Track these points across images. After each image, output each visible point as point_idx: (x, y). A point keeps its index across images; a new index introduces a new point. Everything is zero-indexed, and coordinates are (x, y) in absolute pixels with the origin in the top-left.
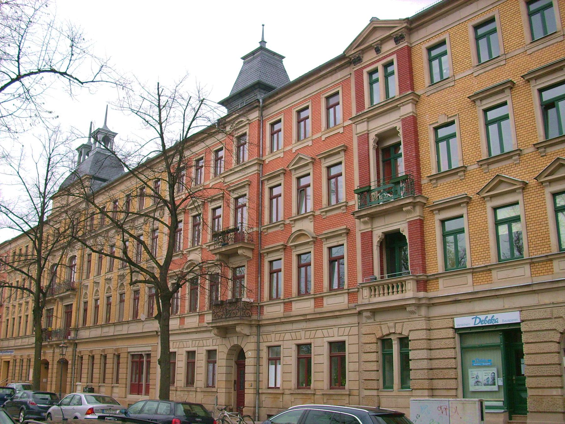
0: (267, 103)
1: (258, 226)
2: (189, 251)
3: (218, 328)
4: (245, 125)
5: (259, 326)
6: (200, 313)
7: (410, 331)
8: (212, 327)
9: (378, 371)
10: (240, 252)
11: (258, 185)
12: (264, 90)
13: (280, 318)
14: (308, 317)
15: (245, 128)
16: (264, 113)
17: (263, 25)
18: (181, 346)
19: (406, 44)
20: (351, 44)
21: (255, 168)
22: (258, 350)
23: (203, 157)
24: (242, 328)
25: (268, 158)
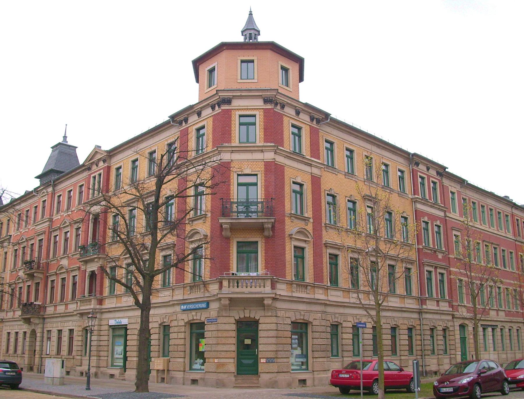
0: (56, 183)
1: (46, 259)
2: (61, 258)
3: (24, 319)
4: (45, 195)
5: (44, 319)
6: (55, 305)
7: (234, 317)
8: (22, 318)
9: (82, 346)
10: (35, 275)
11: (49, 234)
12: (57, 173)
13: (51, 314)
14: (62, 315)
15: (45, 197)
16: (56, 188)
17: (66, 125)
18: (54, 326)
19: (107, 165)
20: (87, 159)
21: (48, 223)
22: (43, 333)
23: (83, 184)
24: (34, 319)
25: (55, 218)
